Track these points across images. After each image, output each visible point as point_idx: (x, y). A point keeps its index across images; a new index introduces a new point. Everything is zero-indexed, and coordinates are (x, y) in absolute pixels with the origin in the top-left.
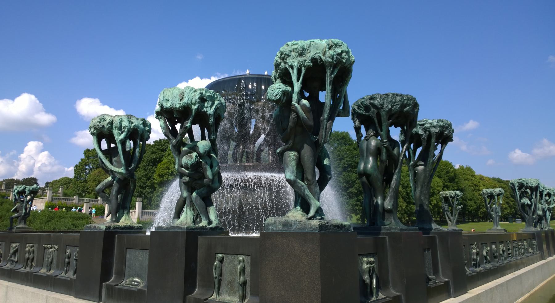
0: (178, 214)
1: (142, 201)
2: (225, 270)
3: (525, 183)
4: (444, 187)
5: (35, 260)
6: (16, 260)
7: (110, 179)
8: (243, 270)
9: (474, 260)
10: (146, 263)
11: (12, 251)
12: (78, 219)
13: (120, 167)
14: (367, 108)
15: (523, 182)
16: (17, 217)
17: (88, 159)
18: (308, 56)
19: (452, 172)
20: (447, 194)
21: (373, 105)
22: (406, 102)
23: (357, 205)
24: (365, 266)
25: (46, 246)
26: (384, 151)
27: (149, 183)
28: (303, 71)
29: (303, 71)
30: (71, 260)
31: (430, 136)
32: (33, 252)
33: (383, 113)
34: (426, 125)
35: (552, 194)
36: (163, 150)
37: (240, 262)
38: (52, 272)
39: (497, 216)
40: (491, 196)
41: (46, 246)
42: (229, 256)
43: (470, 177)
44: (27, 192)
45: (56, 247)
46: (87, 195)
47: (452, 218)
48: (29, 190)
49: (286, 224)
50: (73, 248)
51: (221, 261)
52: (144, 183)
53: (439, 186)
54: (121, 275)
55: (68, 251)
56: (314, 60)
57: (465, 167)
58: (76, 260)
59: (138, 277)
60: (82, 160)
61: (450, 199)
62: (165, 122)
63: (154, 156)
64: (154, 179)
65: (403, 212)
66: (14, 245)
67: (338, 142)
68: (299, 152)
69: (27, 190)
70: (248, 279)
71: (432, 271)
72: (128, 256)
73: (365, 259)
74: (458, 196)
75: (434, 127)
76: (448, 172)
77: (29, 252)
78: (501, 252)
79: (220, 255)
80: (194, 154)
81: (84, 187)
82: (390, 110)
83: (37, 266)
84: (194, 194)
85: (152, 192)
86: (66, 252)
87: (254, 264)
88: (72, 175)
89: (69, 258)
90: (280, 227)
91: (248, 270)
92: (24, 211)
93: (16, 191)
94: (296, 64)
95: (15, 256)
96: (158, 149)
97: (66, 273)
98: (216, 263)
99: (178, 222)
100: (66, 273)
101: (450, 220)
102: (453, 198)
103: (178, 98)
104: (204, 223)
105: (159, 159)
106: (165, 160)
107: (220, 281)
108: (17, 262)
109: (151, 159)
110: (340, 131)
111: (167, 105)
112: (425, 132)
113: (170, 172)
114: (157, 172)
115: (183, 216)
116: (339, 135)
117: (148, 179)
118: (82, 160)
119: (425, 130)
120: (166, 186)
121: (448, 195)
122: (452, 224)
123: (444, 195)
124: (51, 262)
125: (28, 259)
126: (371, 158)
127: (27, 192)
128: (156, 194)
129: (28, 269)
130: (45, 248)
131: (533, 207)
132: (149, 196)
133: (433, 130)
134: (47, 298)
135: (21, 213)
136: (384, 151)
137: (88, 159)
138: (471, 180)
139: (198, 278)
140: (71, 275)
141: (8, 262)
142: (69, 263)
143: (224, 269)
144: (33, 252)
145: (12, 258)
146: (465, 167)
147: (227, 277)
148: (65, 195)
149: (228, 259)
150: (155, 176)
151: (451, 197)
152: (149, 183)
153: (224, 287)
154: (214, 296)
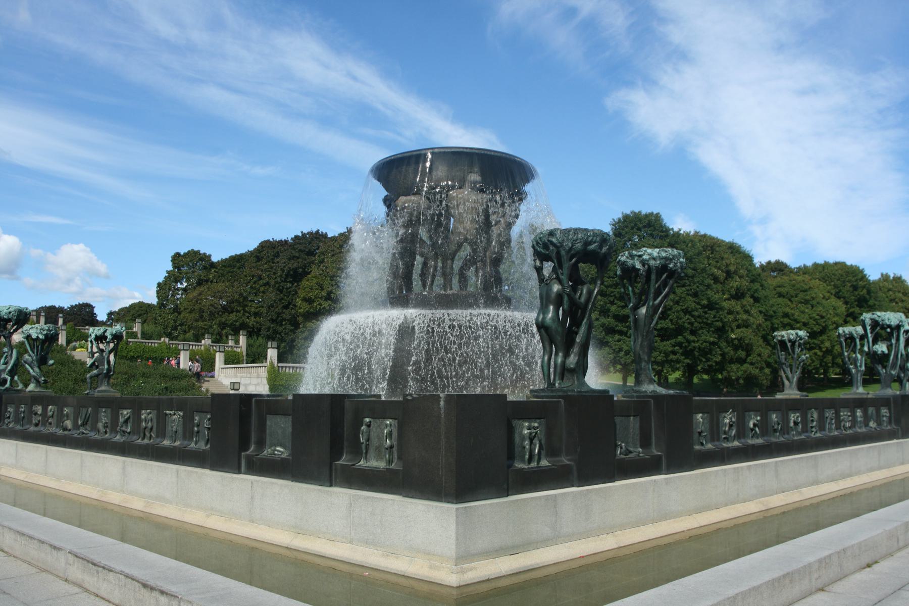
1: (278, 348)
2: (373, 435)
3: (880, 320)
4: (847, 316)
5: (154, 429)
6: (129, 430)
8: (390, 434)
9: (725, 433)
10: (290, 430)
11: (121, 420)
12: (174, 378)
14: (545, 246)
15: (877, 319)
16: (97, 376)
17: (179, 269)
19: (864, 287)
20: (783, 336)
21: (552, 243)
22: (590, 239)
23: (674, 353)
24: (526, 431)
25: (168, 412)
26: (566, 298)
27: (287, 315)
30: (201, 428)
31: (649, 271)
33: (563, 253)
34: (644, 257)
36: (311, 253)
37: (387, 425)
38: (177, 443)
39: (858, 371)
40: (851, 339)
41: (168, 412)
42: (377, 420)
43: (901, 295)
45: (181, 414)
46: (182, 337)
47: (790, 375)
48: (112, 334)
50: (203, 415)
51: (369, 426)
52: (279, 314)
53: (837, 315)
54: (261, 444)
55: (197, 418)
57: (892, 276)
58: (209, 429)
59: (281, 446)
60: (168, 272)
61: (789, 345)
63: (294, 265)
64: (295, 306)
65: (764, 365)
66: (125, 412)
67: (639, 233)
69: (108, 334)
70: (395, 443)
71: (638, 443)
72: (268, 423)
73: (527, 424)
74: (801, 339)
75: (654, 259)
76: (855, 288)
78: (792, 424)
79: (367, 420)
81: (175, 321)
82: (571, 249)
83: (157, 436)
85: (293, 331)
86: (193, 419)
87: (400, 428)
88: (152, 298)
89: (198, 426)
92: (106, 366)
93: (93, 336)
95: (127, 426)
96: (300, 251)
97: (196, 444)
98: (364, 427)
100: (196, 444)
101: (788, 379)
102: (793, 343)
105: (304, 269)
106: (315, 271)
107: (367, 447)
108: (129, 433)
109: (289, 272)
110: (643, 212)
112: (644, 266)
113: (324, 294)
114: (302, 294)
116: (640, 220)
117: (286, 307)
118: (168, 272)
119: (643, 263)
120: (318, 320)
121: (786, 338)
122: (790, 386)
123: (779, 338)
125: (146, 428)
126: (551, 307)
127: (109, 337)
128: (301, 335)
129: (146, 441)
130: (166, 414)
131: (892, 358)
132: (288, 339)
133: (652, 263)
134: (177, 471)
135: (103, 370)
136: (566, 298)
137: (179, 269)
138: (903, 301)
139: (346, 444)
140: (202, 446)
141: (116, 432)
142: (198, 432)
143: (372, 433)
144: (152, 420)
145: (123, 429)
146: (892, 276)
147: (375, 442)
148: (145, 335)
149: (375, 423)
150: (299, 302)
151: (790, 341)
152: (287, 315)
153: (372, 453)
154: (362, 463)
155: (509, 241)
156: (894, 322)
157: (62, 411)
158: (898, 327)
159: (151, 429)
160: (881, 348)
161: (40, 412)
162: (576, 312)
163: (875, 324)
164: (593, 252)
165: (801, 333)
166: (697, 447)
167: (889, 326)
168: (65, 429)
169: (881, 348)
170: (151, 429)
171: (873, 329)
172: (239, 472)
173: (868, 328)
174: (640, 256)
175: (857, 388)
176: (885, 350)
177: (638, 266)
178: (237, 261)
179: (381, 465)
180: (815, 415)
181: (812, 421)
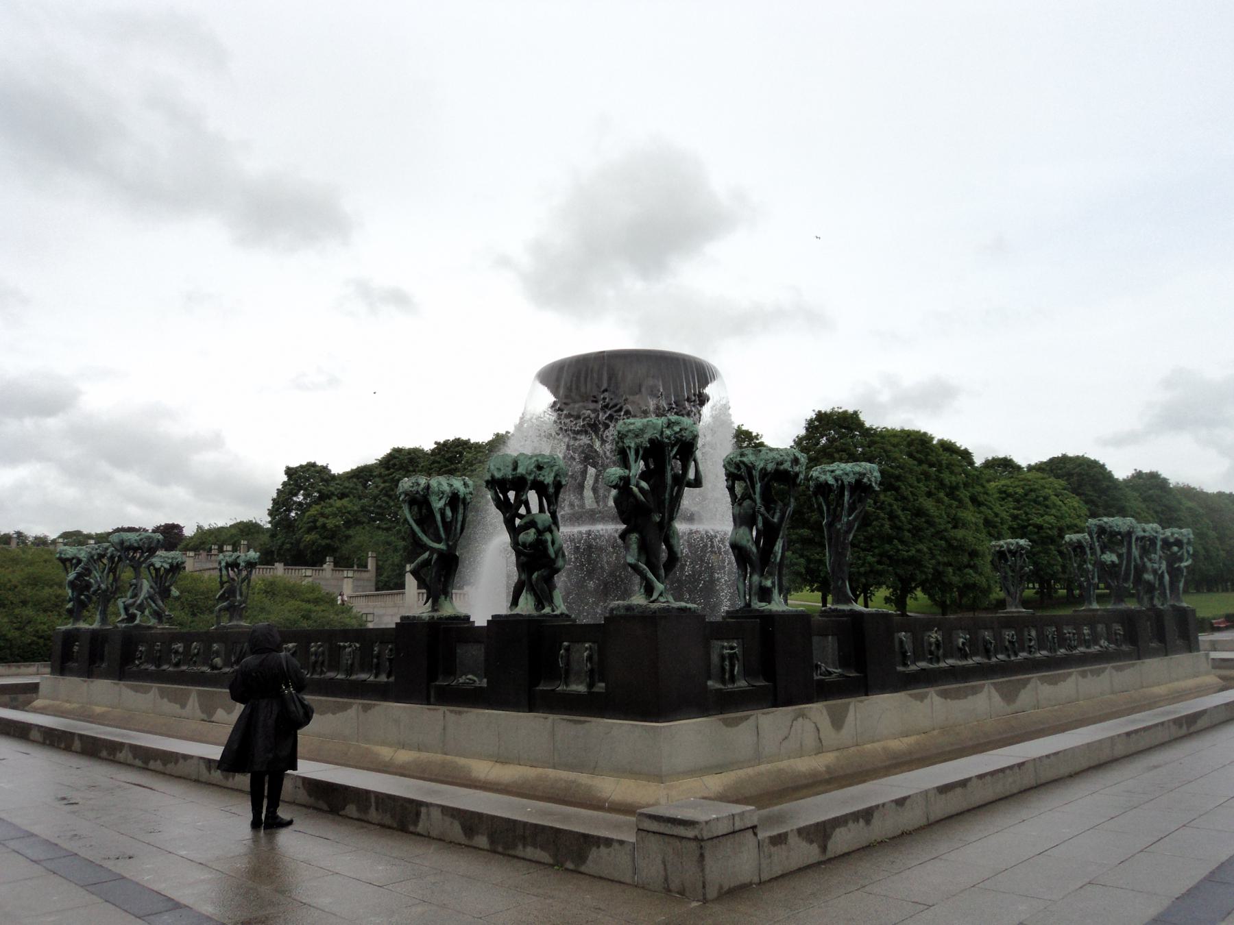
0: (515, 602)
7: (426, 555)
8: (590, 658)
13: (439, 542)
14: (738, 466)
18: (647, 436)
21: (743, 463)
28: (641, 452)
29: (641, 452)
32: (323, 653)
33: (756, 473)
35: (1185, 541)
44: (242, 564)
49: (629, 608)
56: (651, 441)
62: (496, 493)
68: (640, 533)
77: (316, 654)
79: (566, 644)
80: (532, 531)
84: (535, 575)
88: (263, 519)
90: (623, 612)
91: (596, 657)
94: (633, 445)
99: (517, 611)
100: (376, 676)
103: (511, 467)
104: (547, 610)
111: (498, 475)
115: (522, 600)
119: (836, 479)
124: (352, 665)
127: (242, 564)
142: (378, 664)
151: (1010, 551)
155: (687, 448)
156: (1124, 529)
157: (210, 647)
158: (1129, 534)
159: (323, 663)
160: (1110, 557)
161: (181, 650)
162: (769, 534)
163: (1102, 530)
164: (786, 472)
165: (1022, 542)
166: (900, 669)
167: (1119, 533)
168: (214, 667)
169: (1110, 557)
170: (323, 663)
171: (1099, 537)
172: (429, 703)
173: (1095, 536)
174: (833, 471)
175: (1090, 603)
176: (1114, 558)
177: (831, 481)
178: (362, 474)
179: (581, 688)
180: (1033, 633)
181: (1030, 640)
